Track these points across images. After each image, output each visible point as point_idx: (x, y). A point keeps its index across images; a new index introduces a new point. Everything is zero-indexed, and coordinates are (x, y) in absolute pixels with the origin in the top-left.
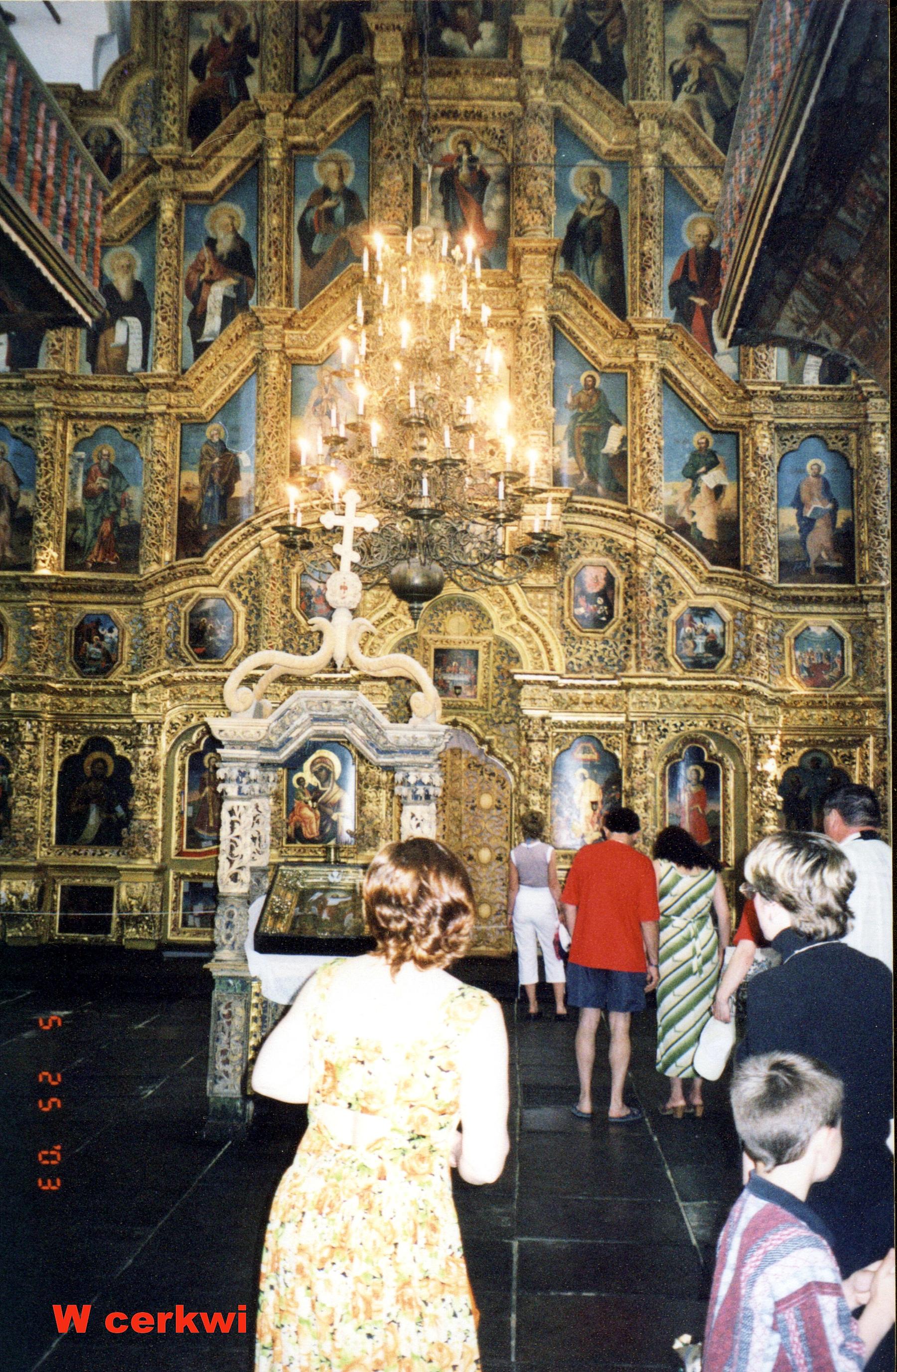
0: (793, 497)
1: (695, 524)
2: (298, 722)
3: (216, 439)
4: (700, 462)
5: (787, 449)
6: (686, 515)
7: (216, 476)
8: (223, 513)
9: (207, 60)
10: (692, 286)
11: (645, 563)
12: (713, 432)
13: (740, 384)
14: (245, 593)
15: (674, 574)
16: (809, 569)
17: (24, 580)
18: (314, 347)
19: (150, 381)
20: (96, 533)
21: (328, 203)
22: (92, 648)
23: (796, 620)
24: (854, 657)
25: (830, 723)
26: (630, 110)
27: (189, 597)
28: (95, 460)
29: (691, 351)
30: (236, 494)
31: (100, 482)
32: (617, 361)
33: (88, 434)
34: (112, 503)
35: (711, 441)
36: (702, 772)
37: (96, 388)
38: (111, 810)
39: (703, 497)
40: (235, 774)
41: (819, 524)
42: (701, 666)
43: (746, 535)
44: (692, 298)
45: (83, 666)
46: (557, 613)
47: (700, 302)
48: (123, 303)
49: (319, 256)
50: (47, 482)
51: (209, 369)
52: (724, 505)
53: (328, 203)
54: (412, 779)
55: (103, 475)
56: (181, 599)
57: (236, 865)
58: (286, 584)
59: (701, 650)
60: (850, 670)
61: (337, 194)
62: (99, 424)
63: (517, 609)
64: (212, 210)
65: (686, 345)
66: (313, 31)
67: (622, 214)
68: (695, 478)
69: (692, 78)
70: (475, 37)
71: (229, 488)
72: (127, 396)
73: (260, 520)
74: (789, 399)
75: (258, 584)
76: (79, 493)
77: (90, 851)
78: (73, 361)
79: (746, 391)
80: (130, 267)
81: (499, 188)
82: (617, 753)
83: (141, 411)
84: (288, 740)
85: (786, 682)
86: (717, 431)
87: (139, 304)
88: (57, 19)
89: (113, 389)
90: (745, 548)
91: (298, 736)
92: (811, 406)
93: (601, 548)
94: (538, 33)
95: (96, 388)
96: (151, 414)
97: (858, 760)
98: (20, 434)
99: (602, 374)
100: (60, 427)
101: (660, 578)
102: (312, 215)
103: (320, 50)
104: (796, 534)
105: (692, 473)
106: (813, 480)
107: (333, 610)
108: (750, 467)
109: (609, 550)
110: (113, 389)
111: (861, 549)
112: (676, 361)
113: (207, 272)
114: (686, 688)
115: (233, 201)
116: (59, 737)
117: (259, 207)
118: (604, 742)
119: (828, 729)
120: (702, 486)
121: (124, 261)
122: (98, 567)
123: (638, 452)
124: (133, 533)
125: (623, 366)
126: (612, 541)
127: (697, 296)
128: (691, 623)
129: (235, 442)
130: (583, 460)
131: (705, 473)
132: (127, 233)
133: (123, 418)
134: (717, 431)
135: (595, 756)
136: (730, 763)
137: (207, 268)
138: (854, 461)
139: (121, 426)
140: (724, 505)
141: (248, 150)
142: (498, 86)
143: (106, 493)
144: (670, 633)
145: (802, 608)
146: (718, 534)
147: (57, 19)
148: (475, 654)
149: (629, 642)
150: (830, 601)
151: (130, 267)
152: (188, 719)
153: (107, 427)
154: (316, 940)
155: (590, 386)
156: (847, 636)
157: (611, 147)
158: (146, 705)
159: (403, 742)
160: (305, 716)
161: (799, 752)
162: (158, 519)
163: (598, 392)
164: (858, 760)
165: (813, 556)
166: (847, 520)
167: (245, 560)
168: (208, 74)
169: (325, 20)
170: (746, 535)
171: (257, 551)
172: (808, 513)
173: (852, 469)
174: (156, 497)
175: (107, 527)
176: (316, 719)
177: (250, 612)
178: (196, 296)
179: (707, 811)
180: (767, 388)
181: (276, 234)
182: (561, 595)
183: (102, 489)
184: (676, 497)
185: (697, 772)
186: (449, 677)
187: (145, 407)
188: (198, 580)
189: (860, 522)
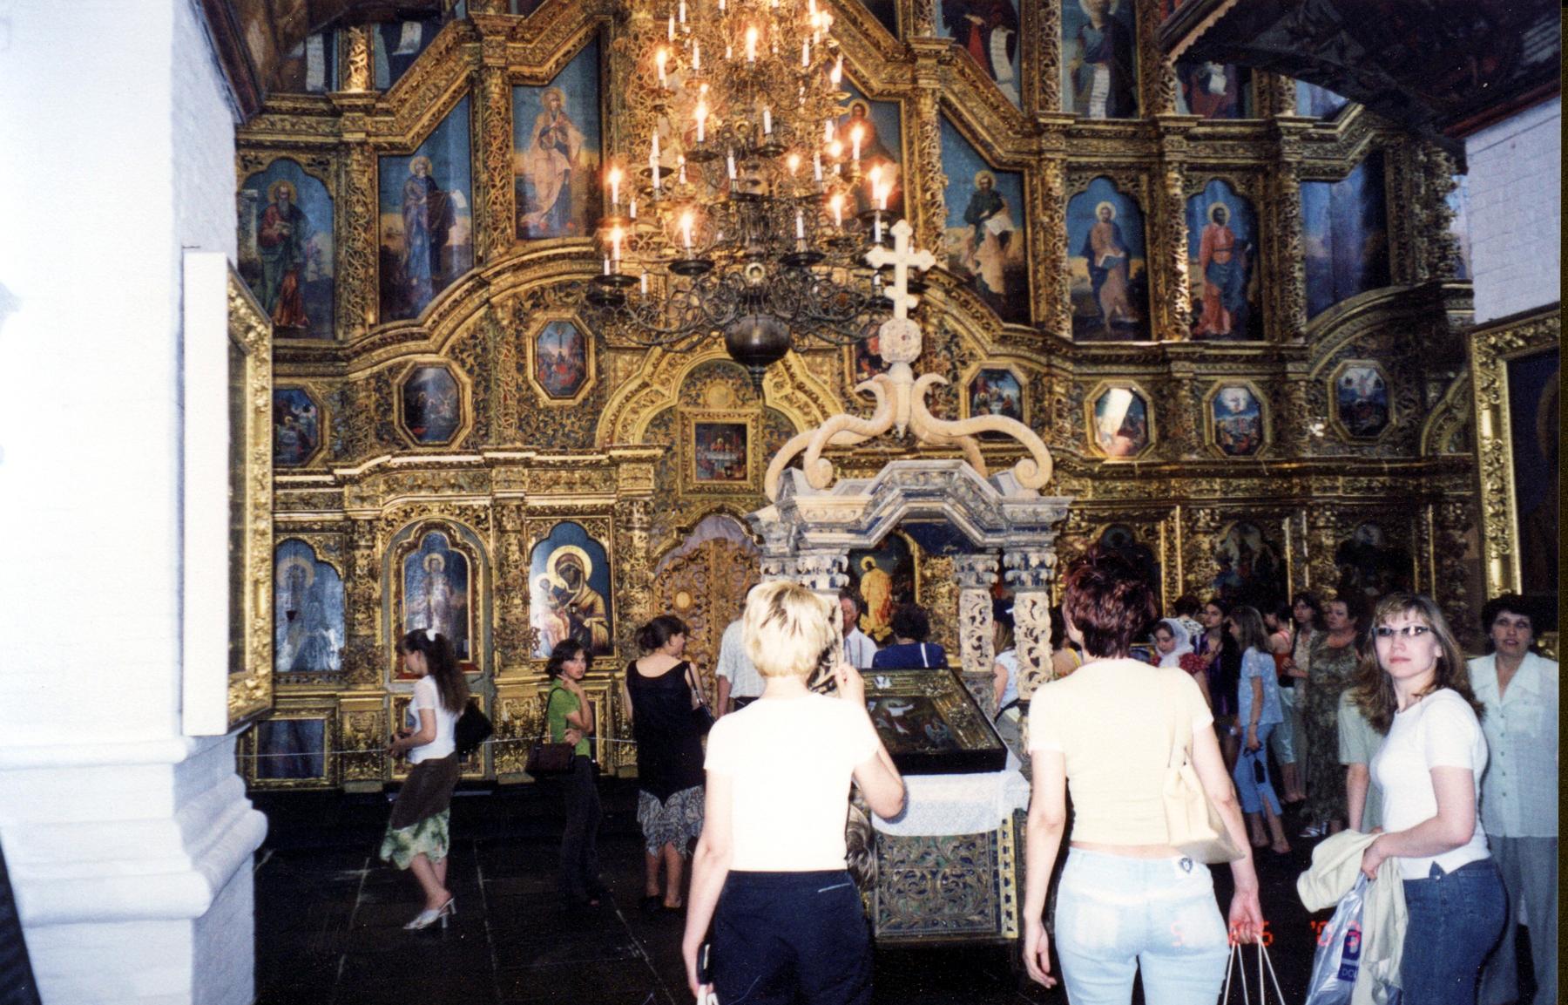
0: (1082, 245)
1: (980, 275)
2: (889, 498)
4: (979, 208)
5: (1076, 190)
6: (970, 266)
11: (935, 321)
12: (994, 170)
14: (470, 360)
16: (1103, 326)
18: (540, 64)
19: (345, 102)
23: (1095, 383)
24: (1157, 421)
25: (1133, 495)
27: (401, 366)
28: (272, 201)
29: (973, 77)
31: (278, 228)
32: (891, 87)
33: (261, 168)
35: (994, 182)
39: (987, 247)
41: (1112, 274)
43: (1037, 288)
46: (838, 379)
47: (976, 20)
51: (415, 89)
52: (1010, 254)
54: (1034, 561)
55: (283, 219)
56: (390, 369)
58: (521, 351)
60: (1153, 434)
63: (792, 376)
65: (967, 70)
72: (312, 120)
73: (490, 272)
74: (1079, 135)
76: (253, 242)
79: (1037, 125)
83: (331, 140)
85: (1088, 451)
86: (999, 169)
89: (294, 112)
92: (1101, 144)
96: (347, 144)
97: (1163, 535)
99: (871, 102)
101: (948, 337)
104: (1088, 286)
105: (974, 218)
106: (1102, 225)
107: (912, 365)
108: (1039, 210)
110: (294, 112)
111: (1157, 303)
112: (956, 88)
119: (1132, 501)
123: (919, 194)
125: (897, 94)
127: (973, 13)
128: (985, 388)
131: (989, 217)
133: (309, 148)
134: (999, 169)
138: (1146, 206)
139: (303, 158)
140: (1010, 254)
144: (962, 400)
145: (1101, 369)
146: (1006, 288)
148: (741, 430)
150: (1130, 360)
152: (407, 514)
153: (283, 158)
154: (925, 756)
156: (1149, 399)
158: (363, 499)
159: (1020, 517)
160: (897, 491)
161: (1101, 529)
162: (361, 271)
164: (1163, 535)
165: (1107, 312)
166: (1140, 270)
167: (470, 321)
170: (1037, 288)
171: (482, 311)
172: (1100, 263)
173: (1142, 214)
174: (359, 245)
176: (908, 495)
177: (476, 385)
180: (1060, 121)
182: (841, 359)
183: (281, 236)
184: (957, 246)
187: (339, 134)
188: (412, 345)
189: (1156, 272)
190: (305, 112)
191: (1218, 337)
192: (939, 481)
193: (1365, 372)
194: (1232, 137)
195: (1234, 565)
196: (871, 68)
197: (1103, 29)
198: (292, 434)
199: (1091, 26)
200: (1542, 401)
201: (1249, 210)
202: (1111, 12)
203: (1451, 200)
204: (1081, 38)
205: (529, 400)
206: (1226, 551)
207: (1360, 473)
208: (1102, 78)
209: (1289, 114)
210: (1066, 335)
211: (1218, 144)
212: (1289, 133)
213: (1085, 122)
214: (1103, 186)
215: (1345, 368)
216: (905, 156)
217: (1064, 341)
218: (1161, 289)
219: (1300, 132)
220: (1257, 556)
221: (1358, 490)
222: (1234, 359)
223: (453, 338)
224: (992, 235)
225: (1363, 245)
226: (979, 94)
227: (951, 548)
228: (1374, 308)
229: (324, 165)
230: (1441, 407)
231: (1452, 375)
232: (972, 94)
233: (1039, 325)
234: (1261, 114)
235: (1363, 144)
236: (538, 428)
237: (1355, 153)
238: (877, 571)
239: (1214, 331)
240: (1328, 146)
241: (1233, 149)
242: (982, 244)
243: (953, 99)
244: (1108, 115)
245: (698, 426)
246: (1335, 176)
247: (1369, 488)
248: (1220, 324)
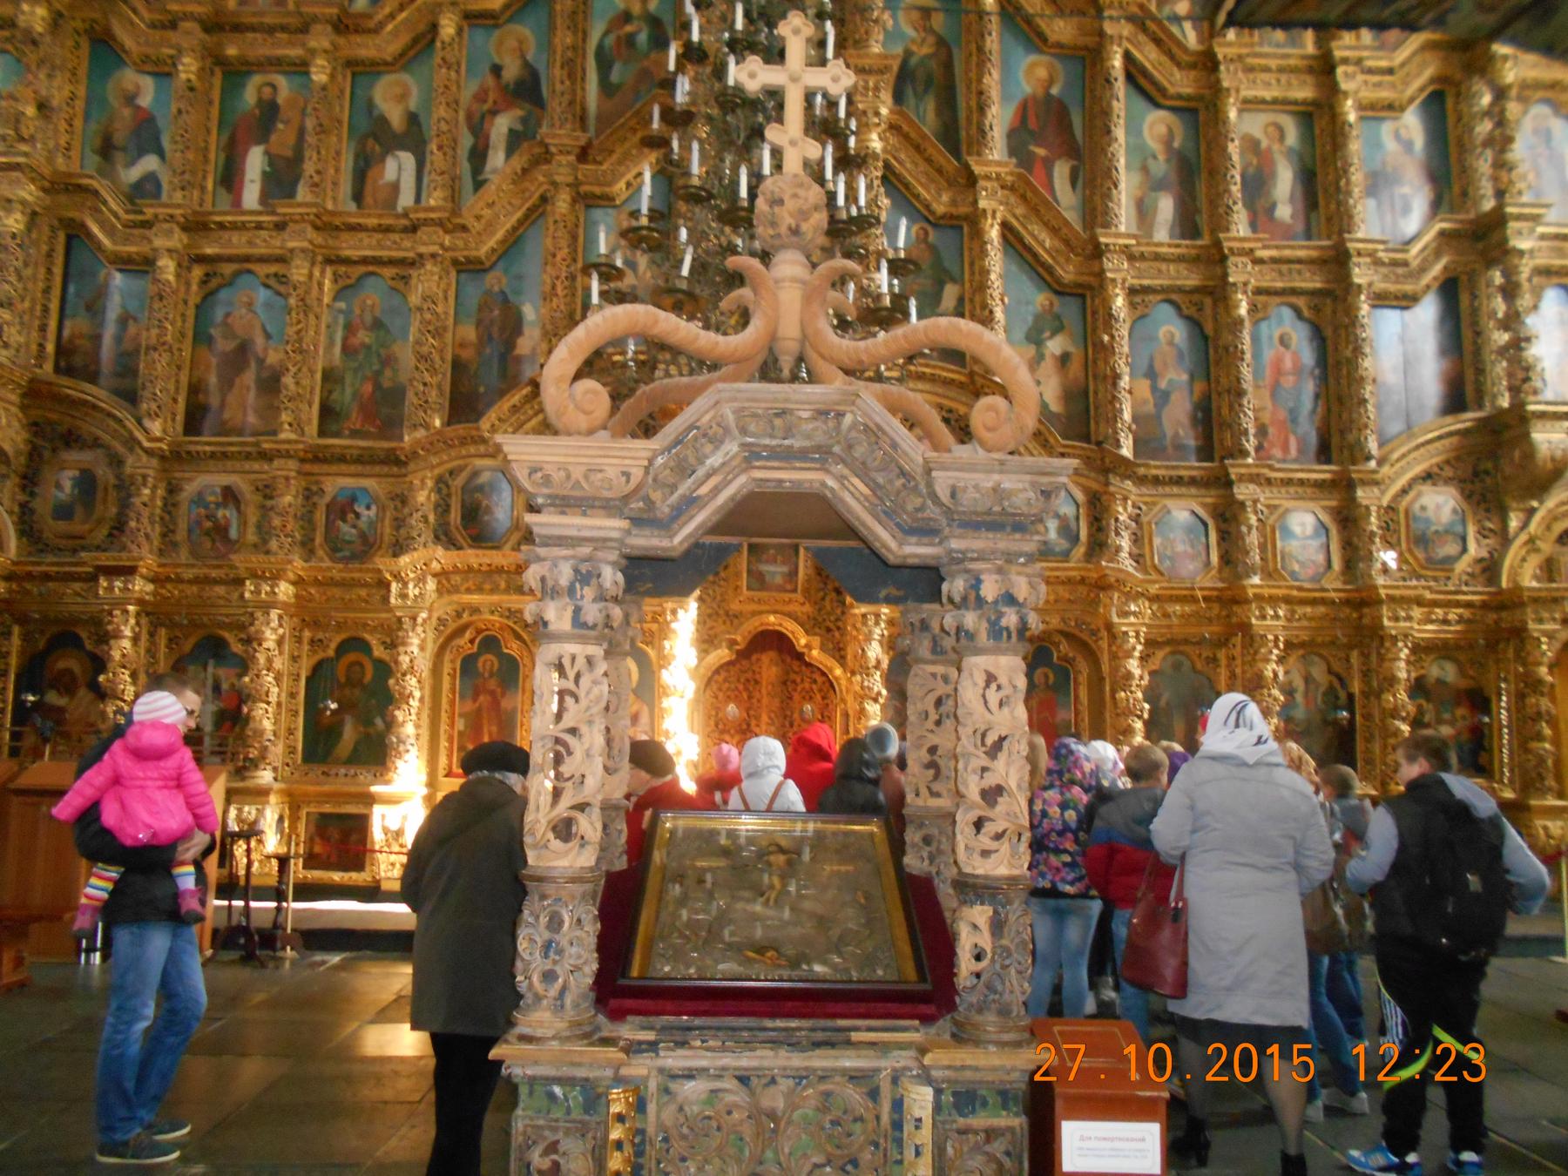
2: (715, 460)
3: (496, 289)
7: (495, 330)
8: (503, 374)
10: (1031, 133)
17: (266, 446)
20: (355, 395)
21: (629, 28)
22: (345, 528)
27: (461, 469)
28: (357, 311)
30: (518, 351)
31: (363, 337)
32: (954, 211)
34: (375, 360)
36: (1051, 676)
38: (368, 722)
40: (565, 574)
44: (1032, 148)
45: (335, 550)
48: (395, 135)
49: (619, 87)
50: (298, 332)
53: (629, 28)
57: (566, 801)
61: (639, 18)
62: (362, 269)
67: (955, 51)
68: (1039, 343)
71: (510, 344)
72: (396, 237)
76: (337, 350)
77: (343, 771)
78: (334, 199)
80: (403, 97)
84: (690, 503)
86: (1059, 290)
87: (413, 137)
90: (1097, 423)
91: (716, 491)
97: (1223, 662)
98: (272, 282)
99: (935, 225)
100: (317, 273)
102: (610, 41)
104: (1150, 408)
106: (1166, 348)
111: (1221, 425)
113: (490, 101)
114: (1409, 452)
116: (307, 634)
117: (552, 28)
120: (1047, 353)
121: (398, 90)
122: (355, 434)
124: (396, 396)
126: (950, 411)
127: (1039, 146)
129: (518, 292)
131: (1051, 337)
133: (391, 262)
136: (1083, 667)
137: (492, 97)
140: (1071, 375)
143: (368, 347)
152: (459, 615)
159: (969, 499)
160: (732, 447)
164: (1223, 662)
165: (1169, 433)
172: (1163, 384)
173: (1205, 338)
175: (368, 388)
178: (479, 129)
181: (570, 54)
183: (363, 345)
186: (765, 568)
189: (1219, 394)
191: (1284, 461)
192: (818, 432)
193: (1440, 499)
194: (1299, 261)
195: (1299, 697)
197: (1168, 161)
198: (354, 531)
199: (1155, 157)
201: (1319, 336)
202: (1176, 144)
203: (1530, 321)
204: (1145, 169)
206: (1290, 683)
207: (1435, 604)
208: (1166, 207)
209: (1360, 235)
210: (1127, 451)
211: (1284, 268)
212: (1359, 254)
213: (1148, 244)
214: (1166, 311)
215: (1419, 495)
216: (967, 276)
217: (1124, 459)
218: (1225, 411)
219: (1372, 254)
220: (1322, 689)
221: (1432, 622)
222: (1301, 482)
224: (1053, 355)
227: (894, 592)
228: (1450, 434)
229: (405, 279)
230: (1523, 537)
231: (1535, 504)
233: (1099, 444)
234: (1329, 238)
235: (1437, 269)
237: (1427, 279)
240: (1400, 271)
241: (1299, 272)
242: (1043, 364)
243: (1015, 223)
244: (1171, 237)
246: (1406, 301)
247: (1445, 622)
248: (1286, 448)
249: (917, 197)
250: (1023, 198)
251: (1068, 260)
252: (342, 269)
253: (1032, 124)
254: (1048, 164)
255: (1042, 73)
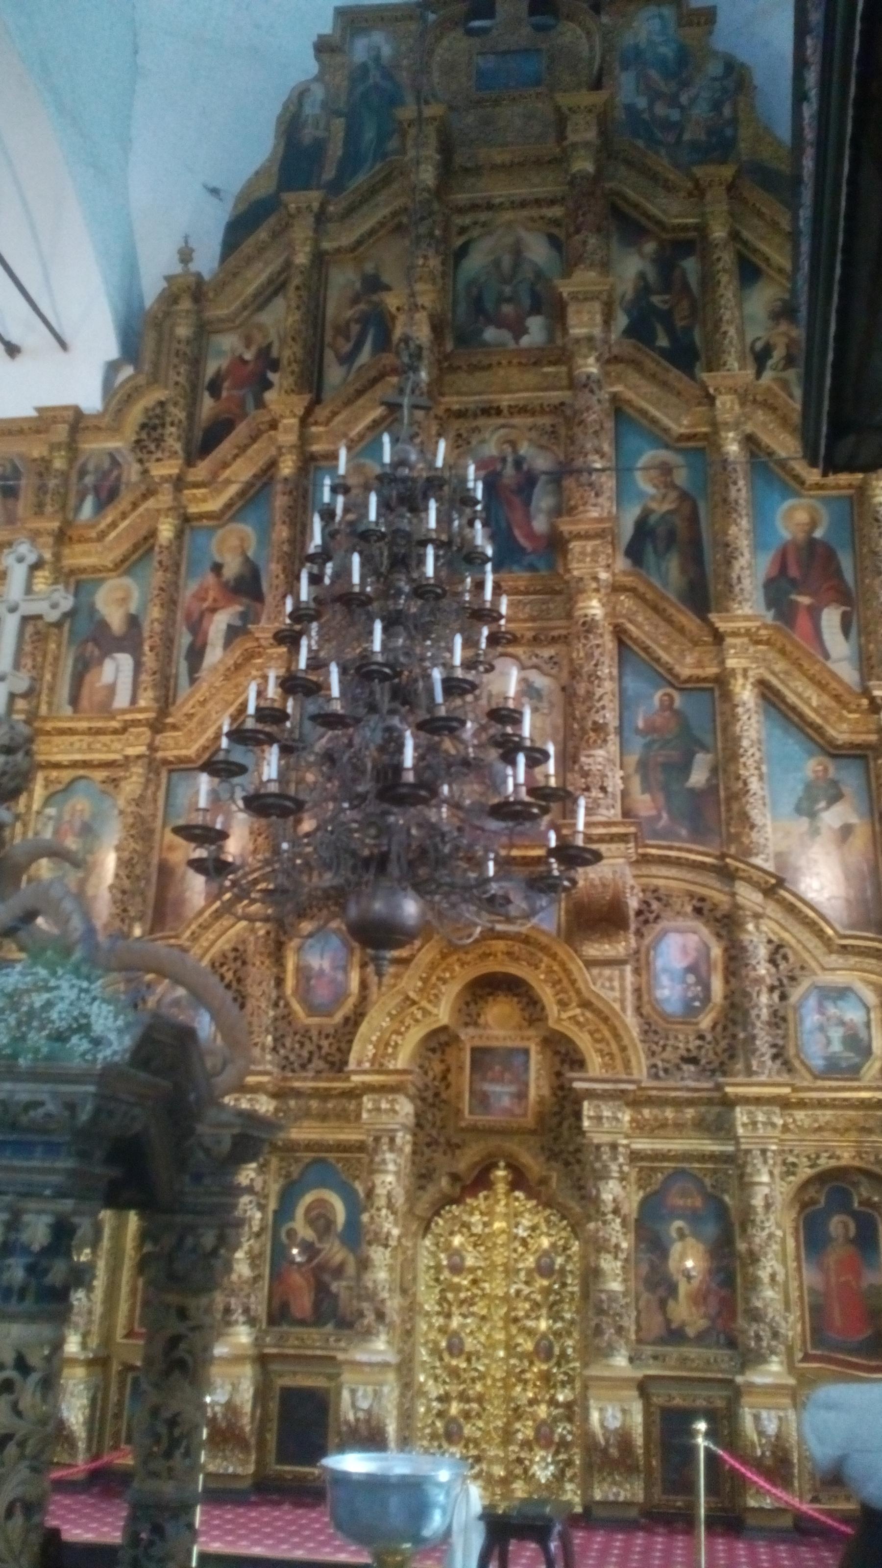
9: (223, 381)
10: (793, 583)
13: (866, 692)
14: (229, 976)
15: (793, 942)
26: (704, 387)
37: (72, 732)
42: (841, 1070)
44: (793, 597)
47: (805, 600)
51: (203, 703)
59: (837, 1047)
64: (220, 532)
65: (789, 648)
66: (341, 341)
69: (778, 354)
70: (519, 331)
75: (244, 963)
81: (550, 487)
82: (727, 1198)
86: (835, 752)
88: (63, 345)
89: (91, 732)
93: (689, 909)
94: (586, 299)
95: (72, 732)
103: (347, 359)
109: (698, 911)
110: (91, 732)
113: (210, 599)
115: (244, 521)
118: (708, 1181)
121: (120, 594)
126: (702, 899)
127: (800, 593)
130: (661, 798)
131: (828, 807)
132: (122, 561)
135: (698, 1202)
137: (212, 594)
141: (261, 462)
142: (546, 375)
147: (63, 345)
149: (734, 1036)
151: (124, 600)
155: (668, 705)
157: (683, 430)
163: (677, 713)
168: (224, 394)
169: (355, 329)
178: (197, 627)
179: (864, 1284)
185: (846, 1226)
190: (99, 732)
196: (675, 654)
200: (809, 52)
205: (287, 1017)
223: (213, 950)
224: (830, 828)
225: (651, 480)
226: (804, 673)
232: (797, 673)
236: (292, 1049)
238: (690, 1241)
239: (258, 924)
243: (775, 681)
245: (474, 1050)
249: (658, 660)
250: (783, 652)
251: (842, 719)
252: (54, 774)
253: (794, 572)
254: (814, 613)
255: (802, 517)
